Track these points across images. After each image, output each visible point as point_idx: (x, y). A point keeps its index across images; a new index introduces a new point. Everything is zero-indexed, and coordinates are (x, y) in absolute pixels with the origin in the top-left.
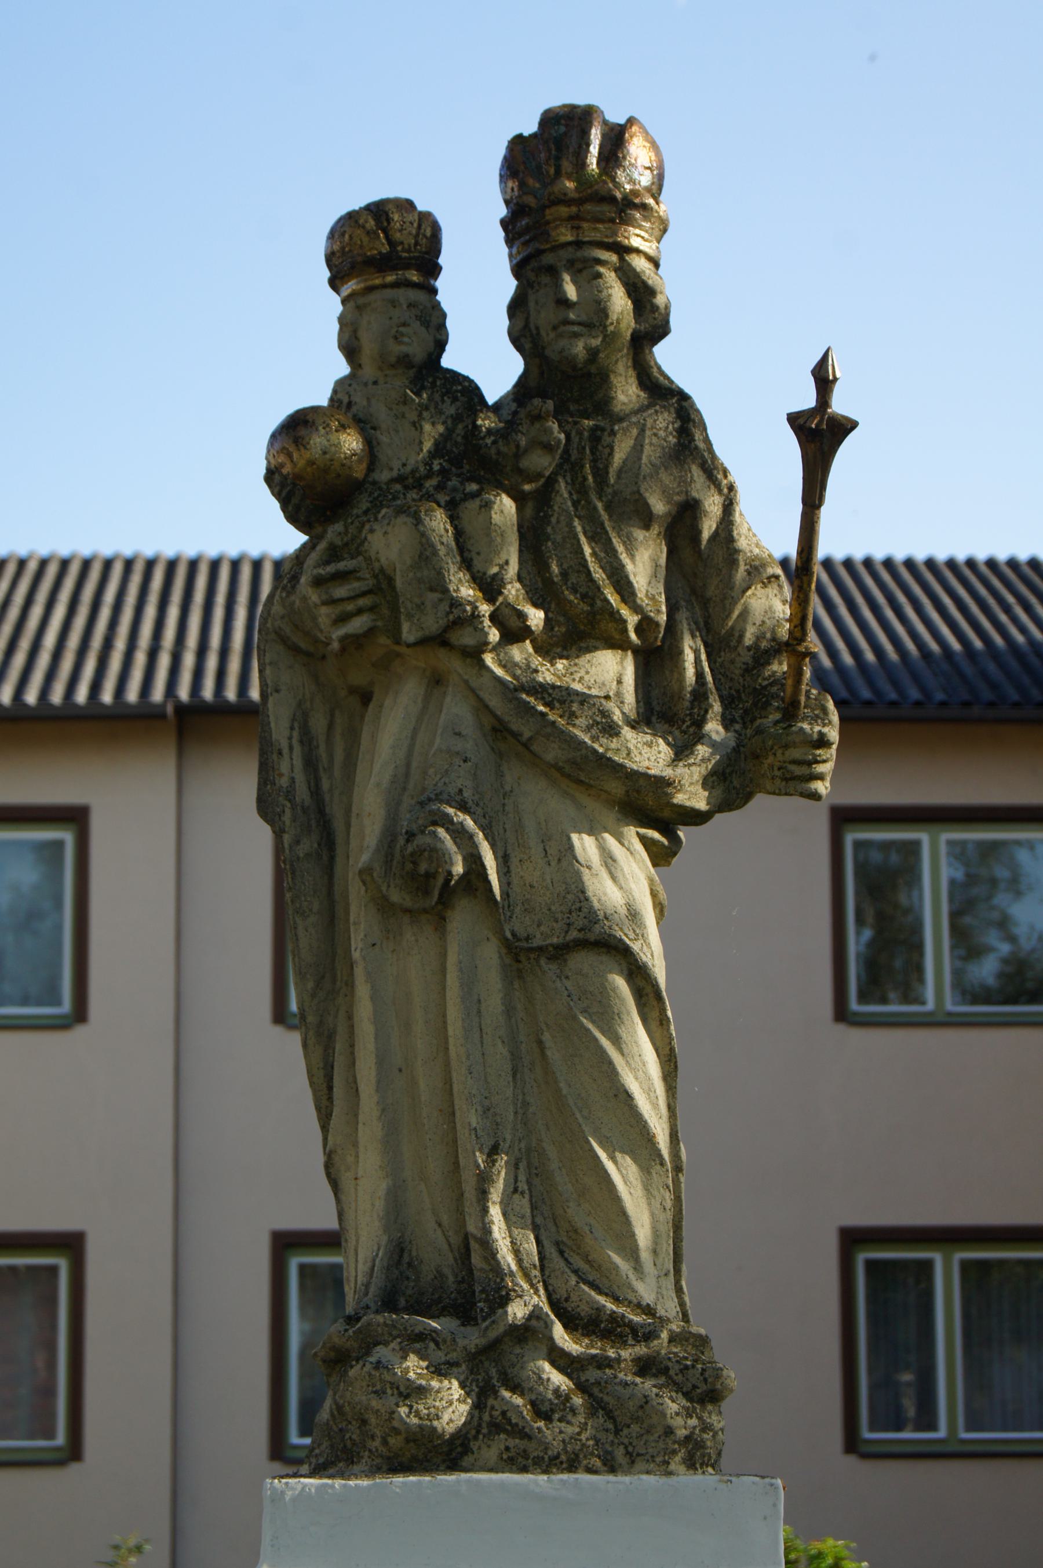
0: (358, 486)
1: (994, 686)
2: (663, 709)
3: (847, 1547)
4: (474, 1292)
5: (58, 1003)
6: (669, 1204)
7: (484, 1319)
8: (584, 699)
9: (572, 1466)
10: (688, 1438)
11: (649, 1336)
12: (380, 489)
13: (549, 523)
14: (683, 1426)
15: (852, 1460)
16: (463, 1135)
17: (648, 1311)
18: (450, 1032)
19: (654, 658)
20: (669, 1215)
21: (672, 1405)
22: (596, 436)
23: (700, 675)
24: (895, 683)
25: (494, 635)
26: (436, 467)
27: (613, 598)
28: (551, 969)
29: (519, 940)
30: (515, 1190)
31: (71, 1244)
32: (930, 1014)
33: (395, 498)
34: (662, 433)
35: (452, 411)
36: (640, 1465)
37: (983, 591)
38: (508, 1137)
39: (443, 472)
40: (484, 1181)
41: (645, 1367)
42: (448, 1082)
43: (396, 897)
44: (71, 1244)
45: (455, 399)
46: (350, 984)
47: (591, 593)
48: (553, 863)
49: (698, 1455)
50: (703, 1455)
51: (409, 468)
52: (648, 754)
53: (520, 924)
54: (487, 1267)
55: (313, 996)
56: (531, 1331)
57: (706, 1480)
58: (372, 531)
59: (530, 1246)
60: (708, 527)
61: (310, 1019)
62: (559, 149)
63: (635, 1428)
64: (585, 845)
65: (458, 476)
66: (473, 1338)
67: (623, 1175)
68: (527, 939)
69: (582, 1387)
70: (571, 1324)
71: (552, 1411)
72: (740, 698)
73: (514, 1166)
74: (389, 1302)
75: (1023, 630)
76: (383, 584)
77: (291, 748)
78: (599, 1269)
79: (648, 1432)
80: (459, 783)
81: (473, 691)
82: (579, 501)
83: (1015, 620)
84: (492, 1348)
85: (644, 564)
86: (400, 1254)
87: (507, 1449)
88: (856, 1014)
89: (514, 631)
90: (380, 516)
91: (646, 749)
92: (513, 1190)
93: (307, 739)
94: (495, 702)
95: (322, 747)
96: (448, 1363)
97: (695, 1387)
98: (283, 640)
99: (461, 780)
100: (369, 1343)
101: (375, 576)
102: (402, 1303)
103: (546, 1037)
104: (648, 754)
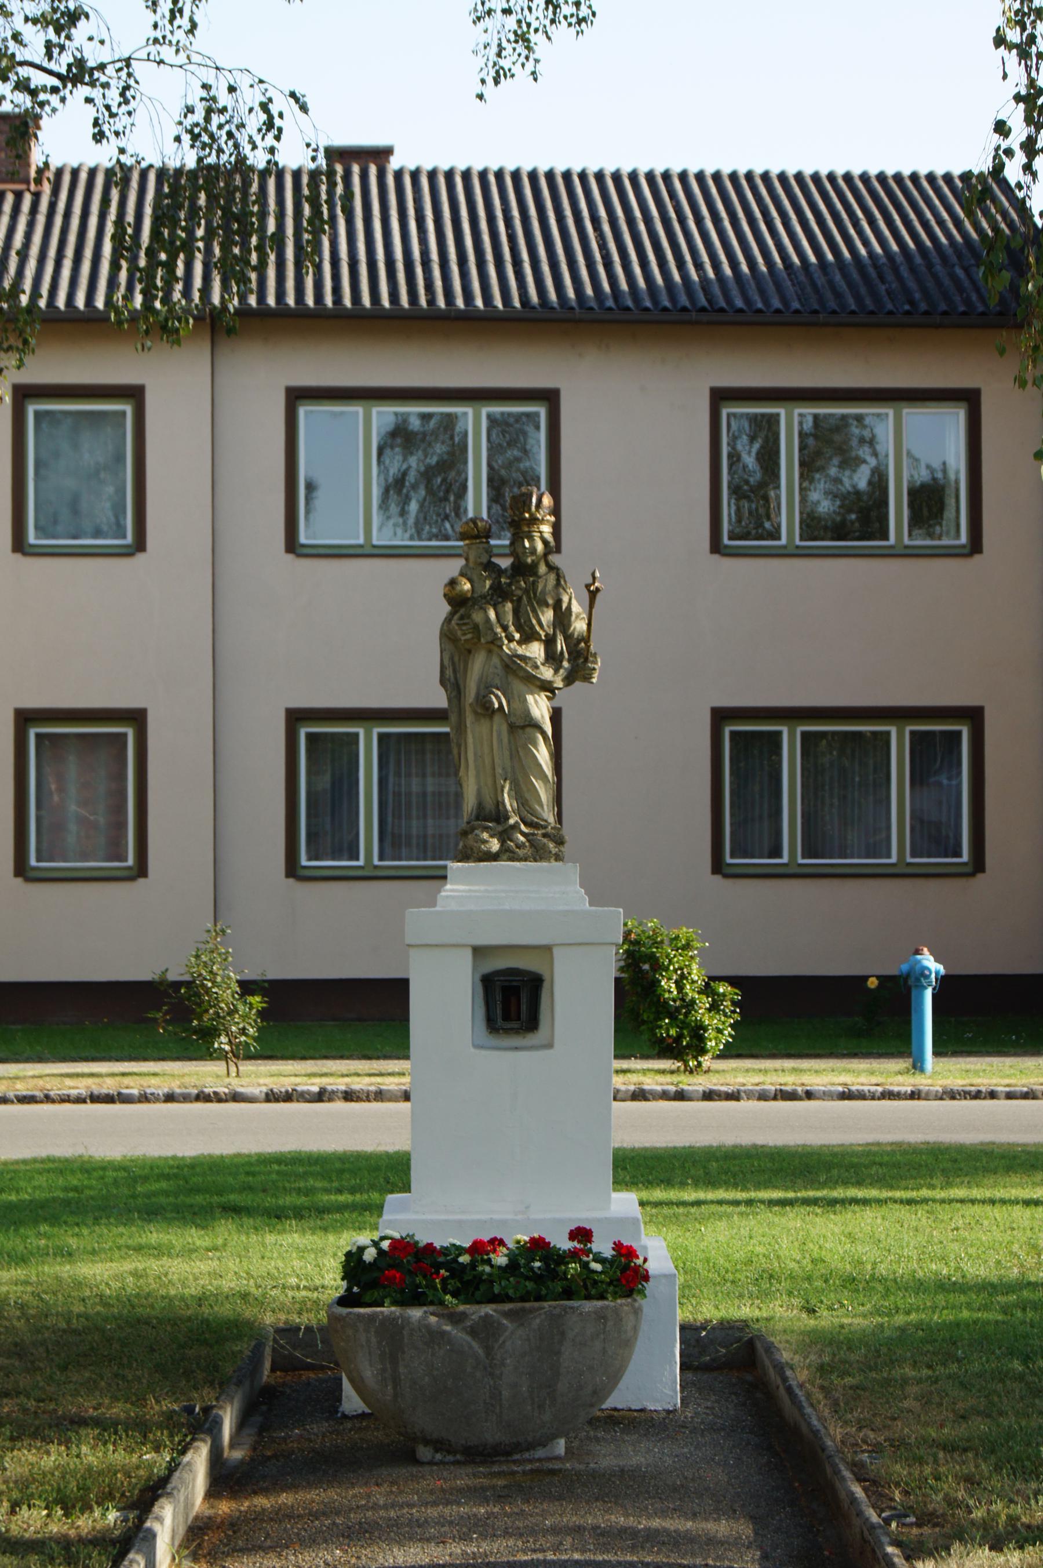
0: (468, 599)
1: (838, 295)
2: (552, 658)
3: (696, 933)
5: (124, 537)
8: (530, 658)
9: (526, 860)
11: (545, 827)
14: (554, 850)
15: (718, 878)
16: (498, 776)
17: (546, 821)
19: (549, 643)
21: (551, 845)
22: (534, 583)
24: (762, 292)
25: (506, 642)
27: (538, 628)
28: (520, 731)
31: (137, 718)
32: (784, 547)
37: (839, 206)
40: (503, 787)
41: (544, 835)
43: (479, 711)
44: (137, 718)
46: (466, 731)
47: (532, 627)
49: (558, 858)
52: (547, 673)
53: (512, 719)
56: (515, 827)
57: (560, 864)
59: (515, 804)
60: (564, 606)
64: (530, 698)
66: (500, 828)
67: (538, 785)
69: (528, 841)
70: (525, 824)
73: (511, 784)
74: (477, 818)
75: (866, 243)
76: (476, 627)
83: (860, 232)
84: (505, 831)
85: (547, 616)
86: (480, 806)
88: (726, 547)
89: (511, 639)
92: (510, 789)
93: (453, 664)
94: (505, 659)
98: (446, 635)
99: (497, 681)
100: (473, 829)
104: (547, 673)
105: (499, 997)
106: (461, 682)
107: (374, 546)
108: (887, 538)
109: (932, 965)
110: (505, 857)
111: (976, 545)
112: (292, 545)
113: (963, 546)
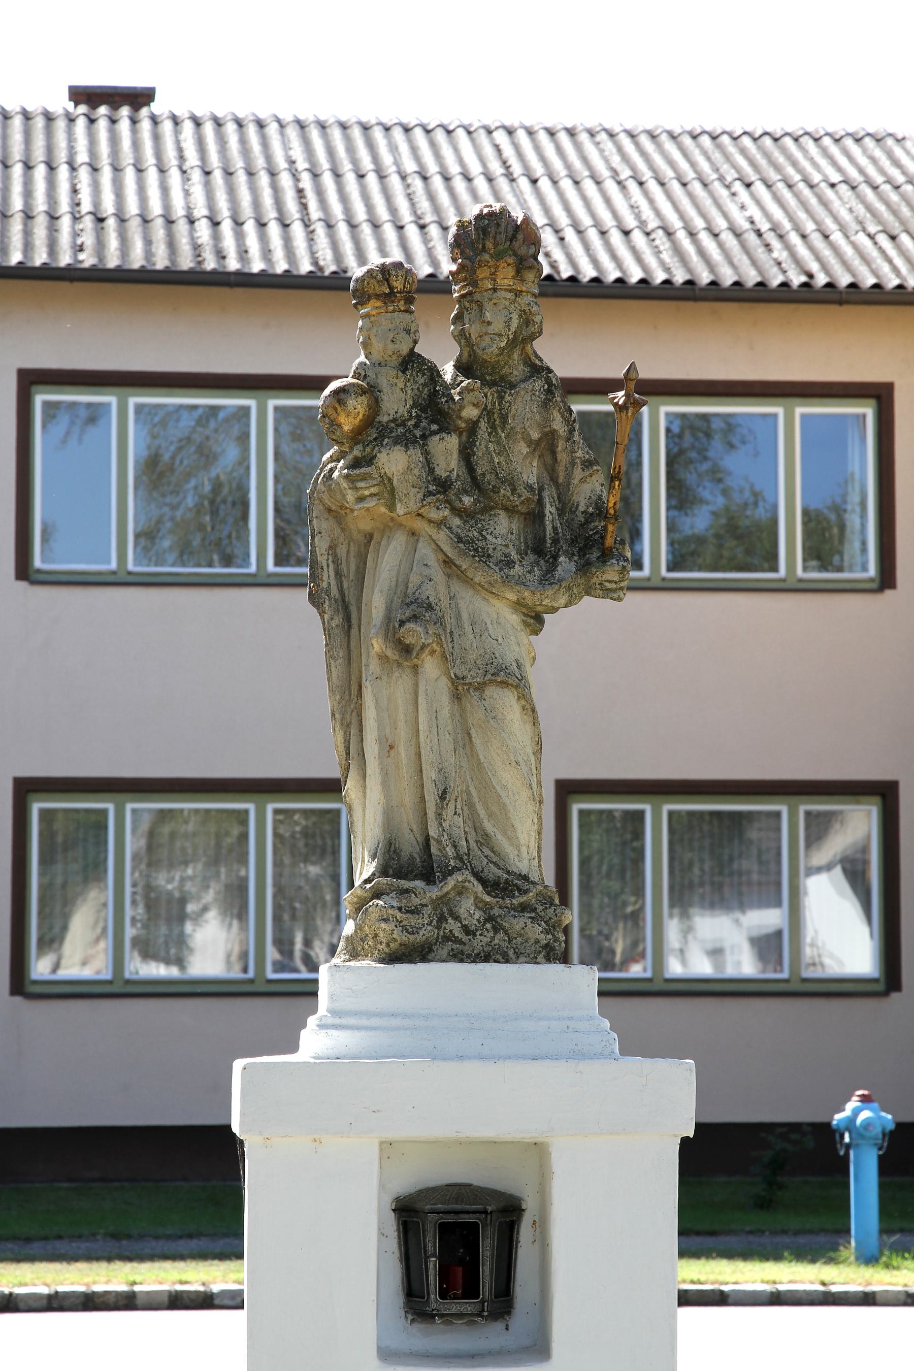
4: (433, 867)
6: (536, 821)
7: (440, 882)
10: (547, 945)
12: (383, 425)
13: (475, 445)
18: (421, 727)
20: (535, 827)
23: (555, 529)
26: (414, 414)
29: (458, 679)
30: (455, 813)
33: (391, 432)
34: (537, 393)
35: (422, 381)
36: (522, 959)
38: (452, 785)
39: (418, 416)
42: (419, 755)
45: (424, 374)
48: (478, 637)
50: (554, 954)
51: (399, 415)
54: (440, 854)
55: (339, 703)
58: (380, 452)
61: (337, 716)
62: (484, 234)
63: (519, 939)
65: (426, 418)
68: (463, 678)
71: (477, 930)
72: (577, 541)
77: (328, 566)
78: (499, 855)
79: (526, 941)
80: (427, 593)
81: (434, 541)
82: (491, 433)
87: (452, 950)
90: (384, 443)
91: (528, 575)
93: (336, 561)
95: (344, 564)
96: (421, 904)
97: (550, 918)
101: (382, 477)
102: (391, 872)
103: (473, 731)
105: (432, 1243)
106: (351, 598)
107: (130, 573)
108: (775, 569)
109: (856, 1113)
110: (444, 952)
111: (887, 578)
112: (24, 570)
113: (871, 580)
